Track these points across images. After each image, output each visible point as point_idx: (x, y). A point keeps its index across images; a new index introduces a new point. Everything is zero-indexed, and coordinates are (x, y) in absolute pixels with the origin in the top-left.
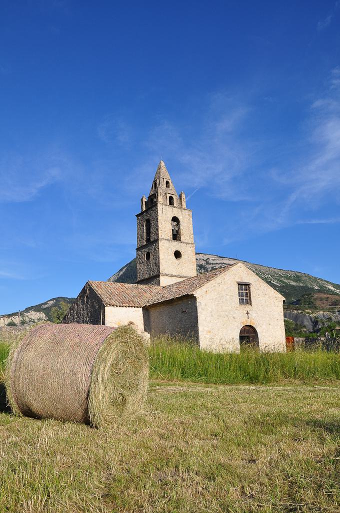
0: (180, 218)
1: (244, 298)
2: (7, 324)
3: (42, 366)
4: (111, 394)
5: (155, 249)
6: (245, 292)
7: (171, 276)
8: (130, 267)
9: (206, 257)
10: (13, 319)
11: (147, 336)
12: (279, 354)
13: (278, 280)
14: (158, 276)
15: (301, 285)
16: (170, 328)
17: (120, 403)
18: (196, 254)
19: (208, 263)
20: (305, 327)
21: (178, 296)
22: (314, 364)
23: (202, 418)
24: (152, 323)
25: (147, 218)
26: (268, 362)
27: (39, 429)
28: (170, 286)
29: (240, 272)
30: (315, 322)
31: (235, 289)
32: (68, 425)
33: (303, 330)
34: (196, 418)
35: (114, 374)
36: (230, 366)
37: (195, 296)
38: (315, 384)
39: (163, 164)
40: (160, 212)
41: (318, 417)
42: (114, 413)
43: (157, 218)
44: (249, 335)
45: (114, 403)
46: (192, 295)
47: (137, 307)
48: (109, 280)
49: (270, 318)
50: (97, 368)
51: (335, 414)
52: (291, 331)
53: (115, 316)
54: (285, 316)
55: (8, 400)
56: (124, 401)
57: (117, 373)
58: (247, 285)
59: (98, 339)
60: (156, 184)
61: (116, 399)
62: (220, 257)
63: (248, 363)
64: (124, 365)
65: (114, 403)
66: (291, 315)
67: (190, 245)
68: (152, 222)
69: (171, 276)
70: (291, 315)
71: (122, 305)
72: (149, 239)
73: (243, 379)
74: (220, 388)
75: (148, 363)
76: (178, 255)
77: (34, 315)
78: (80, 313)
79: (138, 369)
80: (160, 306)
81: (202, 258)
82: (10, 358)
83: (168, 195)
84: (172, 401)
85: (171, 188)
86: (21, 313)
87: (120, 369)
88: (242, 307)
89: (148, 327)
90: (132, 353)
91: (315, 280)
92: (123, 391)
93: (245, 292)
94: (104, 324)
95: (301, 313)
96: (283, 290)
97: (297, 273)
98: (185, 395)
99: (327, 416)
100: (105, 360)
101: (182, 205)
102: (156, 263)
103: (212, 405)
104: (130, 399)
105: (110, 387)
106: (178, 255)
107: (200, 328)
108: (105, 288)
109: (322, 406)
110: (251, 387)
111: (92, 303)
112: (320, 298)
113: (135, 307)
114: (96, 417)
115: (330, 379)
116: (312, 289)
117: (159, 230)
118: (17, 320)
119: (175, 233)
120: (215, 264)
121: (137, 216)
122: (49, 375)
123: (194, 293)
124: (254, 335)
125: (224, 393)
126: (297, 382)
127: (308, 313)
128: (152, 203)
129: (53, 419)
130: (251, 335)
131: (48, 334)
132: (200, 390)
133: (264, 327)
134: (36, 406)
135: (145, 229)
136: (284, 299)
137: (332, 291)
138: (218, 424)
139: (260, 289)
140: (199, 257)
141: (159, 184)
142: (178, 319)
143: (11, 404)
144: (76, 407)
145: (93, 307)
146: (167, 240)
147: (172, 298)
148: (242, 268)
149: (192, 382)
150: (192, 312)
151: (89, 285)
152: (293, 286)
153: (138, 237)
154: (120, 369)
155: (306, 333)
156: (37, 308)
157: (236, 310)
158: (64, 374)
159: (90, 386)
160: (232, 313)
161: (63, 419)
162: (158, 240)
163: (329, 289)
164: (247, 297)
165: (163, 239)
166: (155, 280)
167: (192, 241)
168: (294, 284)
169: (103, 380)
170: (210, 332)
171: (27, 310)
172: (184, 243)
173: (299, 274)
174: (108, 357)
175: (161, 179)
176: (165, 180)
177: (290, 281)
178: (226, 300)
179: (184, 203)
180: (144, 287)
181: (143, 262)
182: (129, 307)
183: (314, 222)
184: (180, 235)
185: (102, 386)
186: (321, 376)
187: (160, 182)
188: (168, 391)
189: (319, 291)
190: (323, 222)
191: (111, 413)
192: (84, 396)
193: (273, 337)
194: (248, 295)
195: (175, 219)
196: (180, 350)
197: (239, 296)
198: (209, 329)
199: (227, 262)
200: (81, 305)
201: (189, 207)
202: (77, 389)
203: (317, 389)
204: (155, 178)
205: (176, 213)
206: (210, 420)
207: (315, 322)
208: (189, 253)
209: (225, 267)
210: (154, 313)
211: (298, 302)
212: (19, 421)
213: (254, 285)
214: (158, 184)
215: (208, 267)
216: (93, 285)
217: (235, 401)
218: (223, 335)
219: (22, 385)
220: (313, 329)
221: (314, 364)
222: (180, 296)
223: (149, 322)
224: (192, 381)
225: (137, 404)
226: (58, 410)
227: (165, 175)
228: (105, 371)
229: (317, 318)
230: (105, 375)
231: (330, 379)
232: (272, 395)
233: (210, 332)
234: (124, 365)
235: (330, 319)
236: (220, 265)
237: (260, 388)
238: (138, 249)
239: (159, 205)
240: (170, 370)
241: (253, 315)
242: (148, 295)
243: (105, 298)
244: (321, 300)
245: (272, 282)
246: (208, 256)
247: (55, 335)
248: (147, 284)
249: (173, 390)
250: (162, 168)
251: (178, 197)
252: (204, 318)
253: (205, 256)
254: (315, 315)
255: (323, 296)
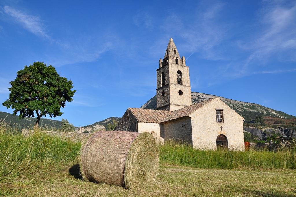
0: (182, 71)
1: (220, 118)
2: (83, 132)
3: (99, 153)
4: (137, 171)
5: (167, 89)
6: (220, 115)
7: (177, 105)
8: (153, 100)
9: (198, 94)
10: (87, 129)
11: (162, 140)
12: (240, 152)
13: (241, 108)
14: (169, 105)
15: (256, 111)
16: (176, 136)
17: (142, 176)
18: (192, 92)
19: (199, 98)
20: (257, 136)
21: (180, 117)
22: (261, 158)
23: (189, 187)
24: (165, 133)
25: (163, 71)
26: (232, 156)
27: (97, 188)
28: (176, 111)
29: (217, 103)
30: (264, 134)
31: (214, 113)
32: (113, 187)
33: (256, 138)
34: (186, 186)
35: (139, 159)
36: (209, 158)
37: (190, 117)
38: (261, 170)
39: (172, 40)
40: (170, 68)
41: (259, 189)
42: (139, 181)
43: (169, 72)
44: (222, 140)
45: (138, 176)
46: (189, 116)
47: (157, 123)
48: (141, 107)
49: (235, 130)
50: (129, 156)
51: (270, 188)
52: (247, 139)
53: (143, 127)
54: (244, 129)
55: (81, 172)
56: (144, 175)
57: (141, 159)
58: (221, 111)
59: (130, 139)
60: (168, 52)
61: (140, 174)
62: (206, 94)
63: (221, 156)
64: (144, 155)
65: (138, 176)
66: (249, 129)
67: (188, 87)
68: (166, 74)
69: (177, 105)
70: (249, 129)
71: (148, 122)
72: (164, 83)
73: (217, 166)
74: (203, 170)
75: (159, 154)
76: (181, 93)
77: (99, 127)
78: (124, 126)
79: (153, 157)
80: (170, 123)
81: (196, 95)
82: (82, 149)
83: (175, 58)
84: (174, 176)
85: (176, 54)
86: (91, 126)
87: (142, 157)
88: (218, 124)
89: (162, 135)
90: (150, 148)
91: (264, 108)
92: (144, 169)
93: (220, 115)
94: (137, 132)
95: (255, 128)
96: (244, 114)
97: (253, 104)
98: (182, 174)
99: (265, 189)
100: (134, 151)
101: (183, 64)
102: (168, 98)
103: (196, 180)
104: (148, 174)
105: (137, 166)
106: (181, 93)
107: (193, 136)
108: (138, 111)
109: (263, 183)
110: (221, 171)
111: (131, 120)
112: (267, 119)
113: (155, 123)
114: (128, 183)
115: (270, 168)
116: (263, 114)
117: (170, 78)
118: (89, 129)
119: (179, 80)
120: (203, 98)
121: (157, 70)
122: (103, 159)
123: (189, 115)
124: (225, 140)
125: (204, 173)
126: (250, 169)
127: (260, 128)
128: (165, 63)
129: (105, 183)
130: (223, 140)
131: (103, 136)
132: (190, 171)
133: (231, 136)
134: (96, 176)
135: (161, 78)
136: (244, 119)
137: (275, 115)
138: (198, 190)
139: (229, 113)
140: (193, 94)
141: (170, 52)
142: (180, 130)
143: (82, 174)
144: (117, 177)
145: (131, 122)
146: (175, 84)
147: (177, 118)
148: (219, 101)
149: (186, 167)
150: (189, 126)
151: (129, 110)
152: (251, 112)
153: (157, 82)
154: (142, 157)
155: (258, 140)
156: (100, 123)
157: (216, 125)
158: (111, 158)
159: (125, 166)
160: (212, 127)
161: (110, 183)
162: (169, 84)
163: (273, 114)
164: (221, 118)
165: (172, 83)
166: (168, 108)
167: (189, 85)
168: (251, 110)
169: (132, 162)
170: (199, 138)
171: (95, 124)
172: (184, 86)
173: (254, 105)
174: (136, 150)
175: (171, 49)
176: (173, 49)
177: (248, 109)
178: (209, 119)
179: (184, 63)
180: (161, 111)
181: (160, 97)
182: (152, 123)
183: (264, 72)
184: (182, 81)
185: (132, 166)
186: (265, 166)
187: (170, 50)
188: (172, 171)
189: (267, 115)
190: (269, 72)
191: (137, 181)
192: (122, 171)
193: (237, 141)
194: (222, 117)
195: (179, 72)
196: (180, 148)
197: (216, 117)
198: (198, 137)
199: (211, 97)
200: (124, 122)
201: (187, 65)
202: (118, 167)
203: (261, 173)
204: (167, 48)
205: (179, 68)
206: (193, 188)
207: (264, 134)
208: (187, 92)
209: (208, 100)
210: (166, 127)
211: (253, 121)
212: (86, 184)
213: (225, 111)
214: (169, 51)
215: (199, 100)
216: (131, 110)
217: (210, 178)
218: (206, 140)
219: (88, 164)
220: (263, 138)
221: (261, 158)
222: (181, 117)
223: (164, 132)
224: (187, 166)
225: (152, 177)
226: (107, 179)
227: (173, 46)
228: (134, 157)
229: (265, 132)
230: (134, 159)
231: (270, 168)
232: (233, 175)
233: (199, 138)
234: (144, 155)
235: (273, 132)
236: (206, 99)
237: (226, 171)
238: (157, 90)
239: (169, 64)
240: (174, 160)
241: (224, 128)
242: (163, 116)
243: (138, 118)
244: (268, 121)
245: (238, 109)
246: (199, 94)
247: (106, 137)
248: (162, 110)
249: (175, 171)
250: (171, 42)
251: (181, 59)
252: (195, 130)
253: (197, 94)
254: (264, 129)
255: (269, 118)
